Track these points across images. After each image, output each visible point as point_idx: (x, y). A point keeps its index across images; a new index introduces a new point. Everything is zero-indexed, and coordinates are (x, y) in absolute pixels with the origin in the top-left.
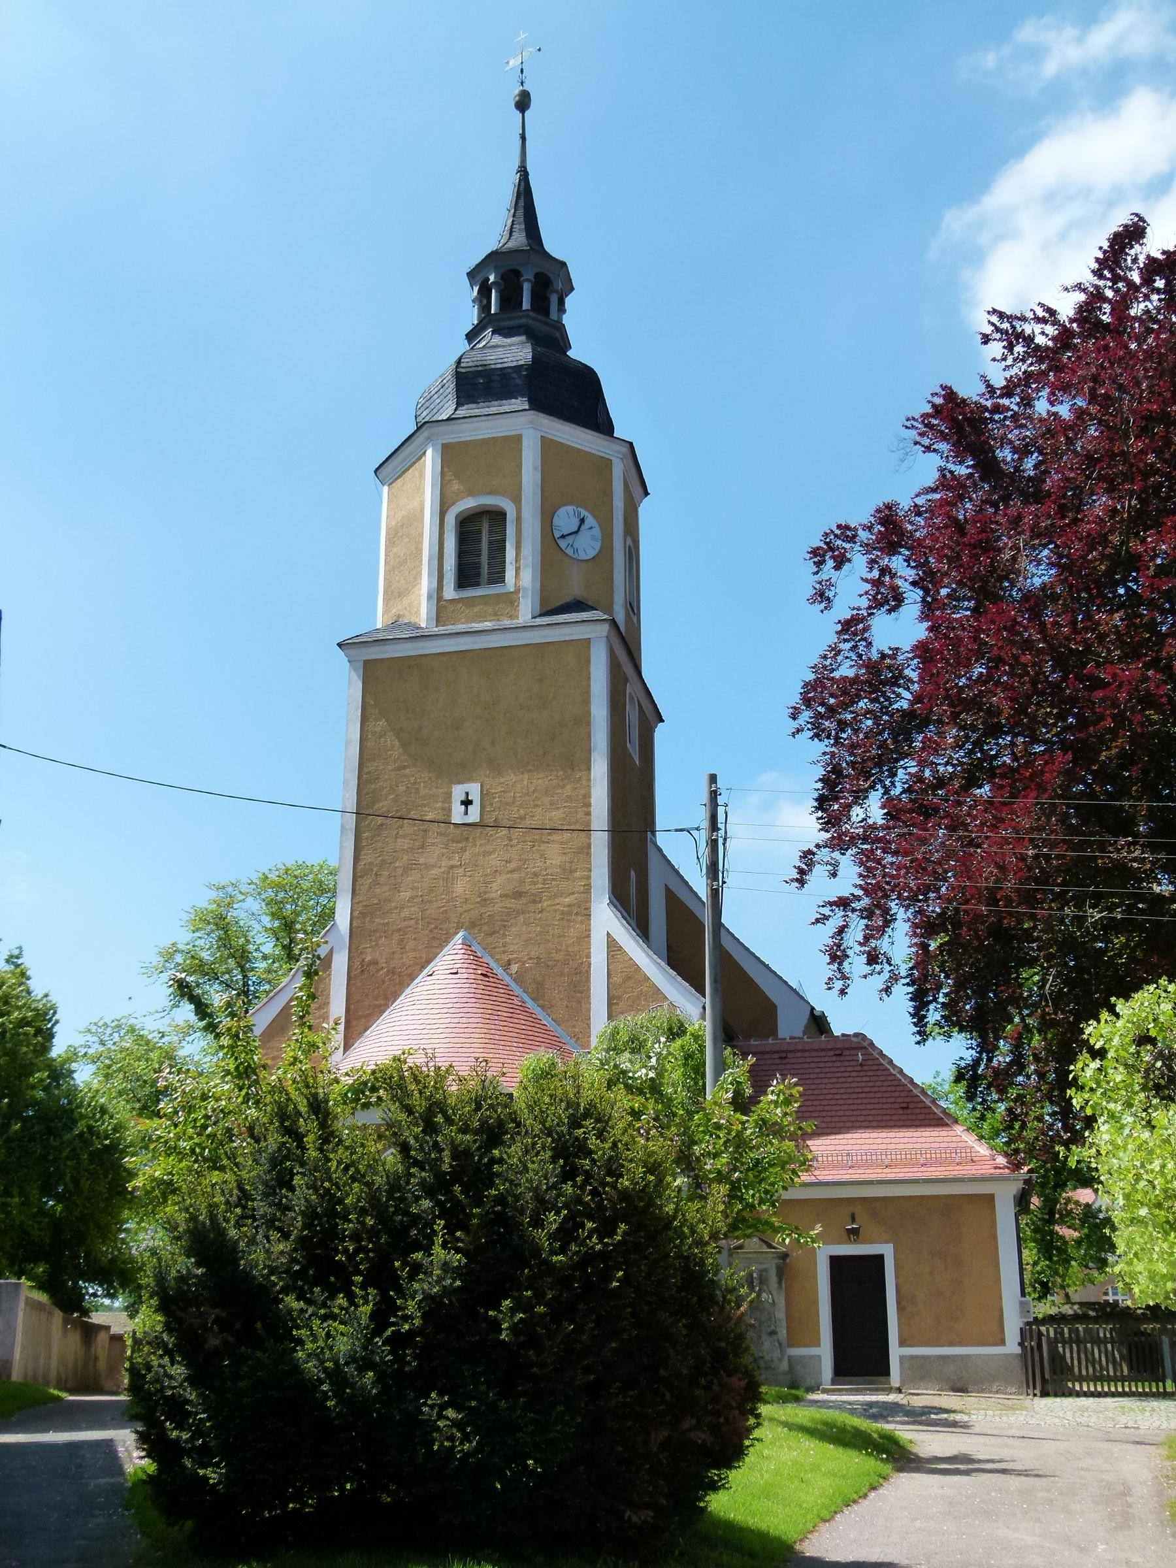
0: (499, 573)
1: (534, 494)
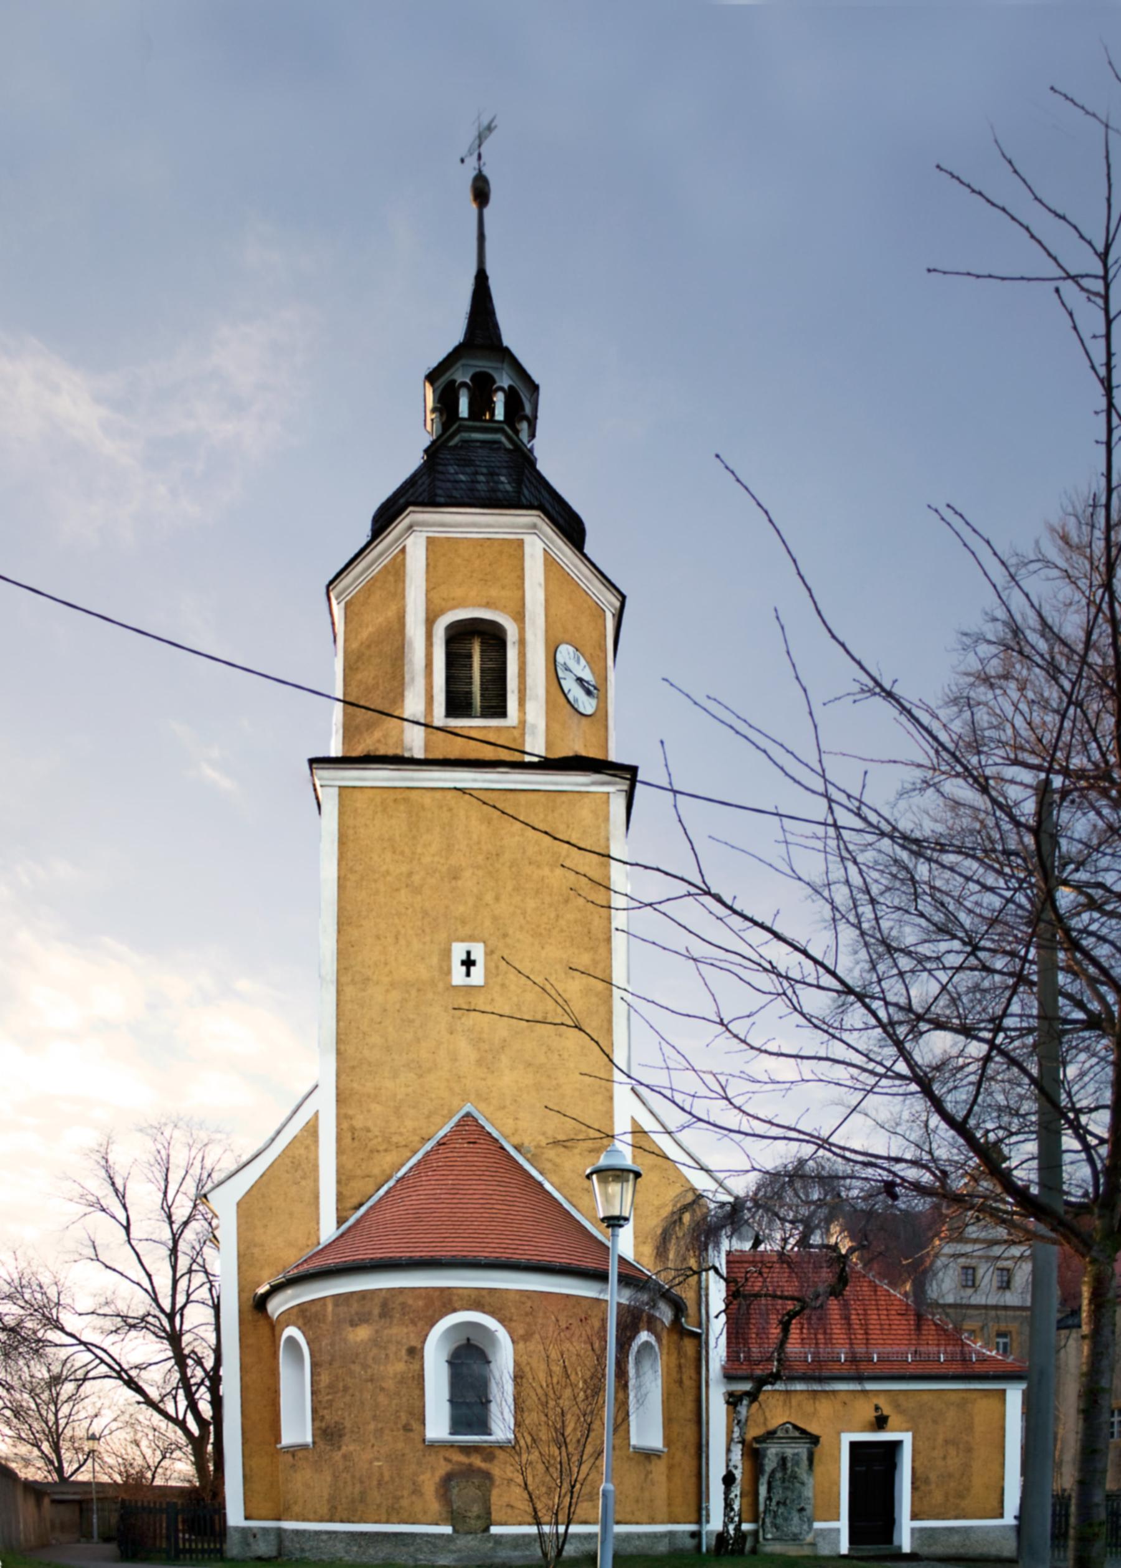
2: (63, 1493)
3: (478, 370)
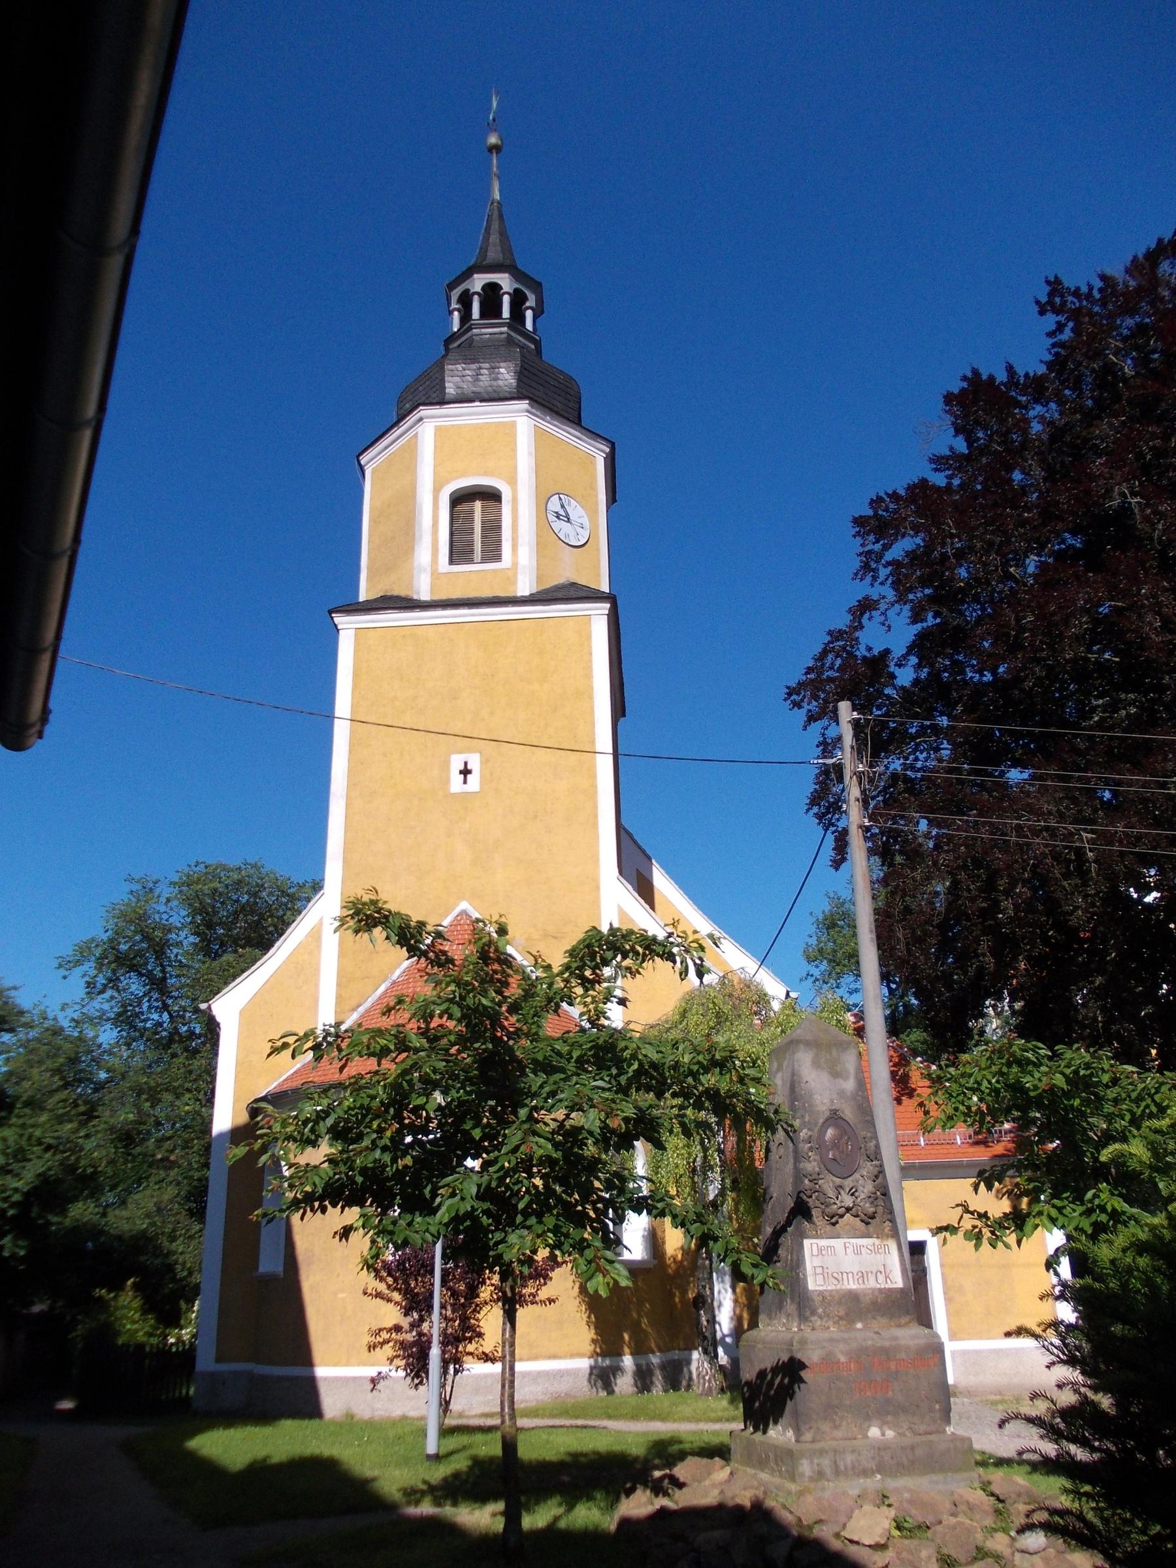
0: (495, 520)
1: (529, 477)
2: (386, 448)
3: (488, 281)
